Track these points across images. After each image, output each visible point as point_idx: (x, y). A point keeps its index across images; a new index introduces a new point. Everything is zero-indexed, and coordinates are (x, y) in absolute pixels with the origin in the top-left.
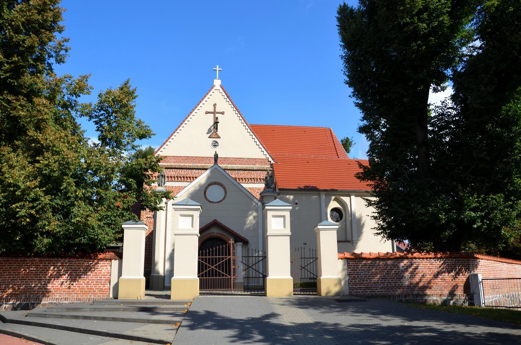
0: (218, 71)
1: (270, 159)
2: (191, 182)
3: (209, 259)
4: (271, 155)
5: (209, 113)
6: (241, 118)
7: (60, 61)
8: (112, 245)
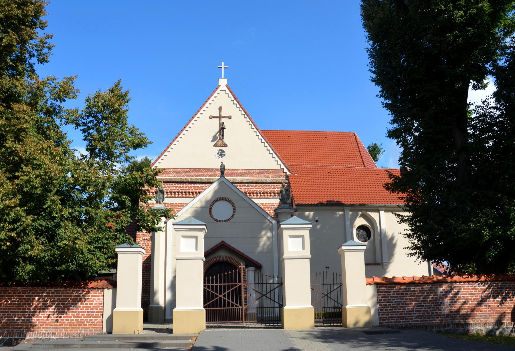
1: (286, 170)
3: (217, 286)
6: (251, 123)
7: (43, 60)
8: (103, 272)
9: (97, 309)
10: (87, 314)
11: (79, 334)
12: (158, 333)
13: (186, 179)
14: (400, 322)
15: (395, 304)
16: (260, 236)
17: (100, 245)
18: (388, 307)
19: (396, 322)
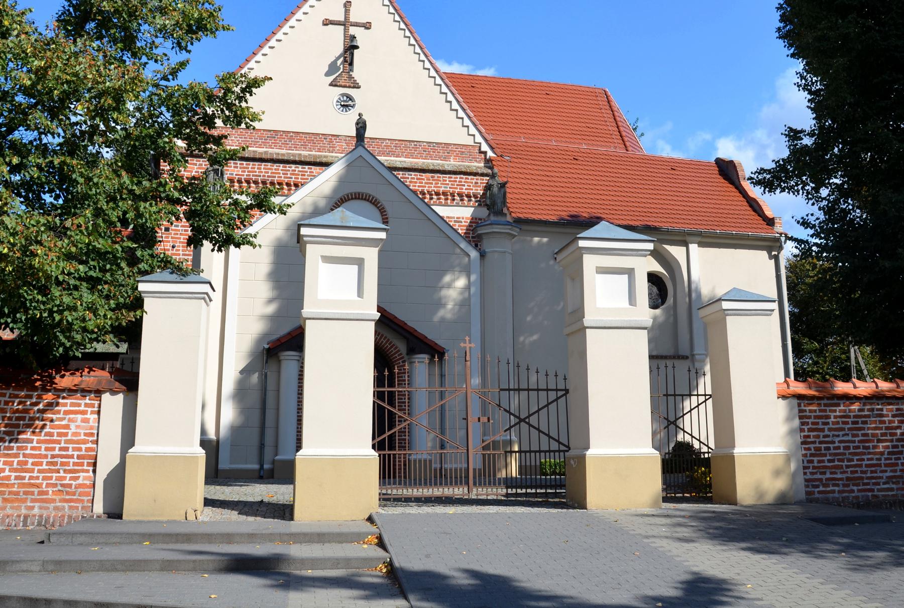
1: (485, 147)
4: (489, 137)
5: (332, 23)
6: (413, 41)
8: (100, 348)
9: (80, 449)
10: (48, 463)
11: (26, 517)
12: (251, 519)
13: (266, 153)
14: (853, 491)
15: (839, 448)
16: (440, 285)
17: (92, 273)
18: (825, 455)
19: (843, 492)
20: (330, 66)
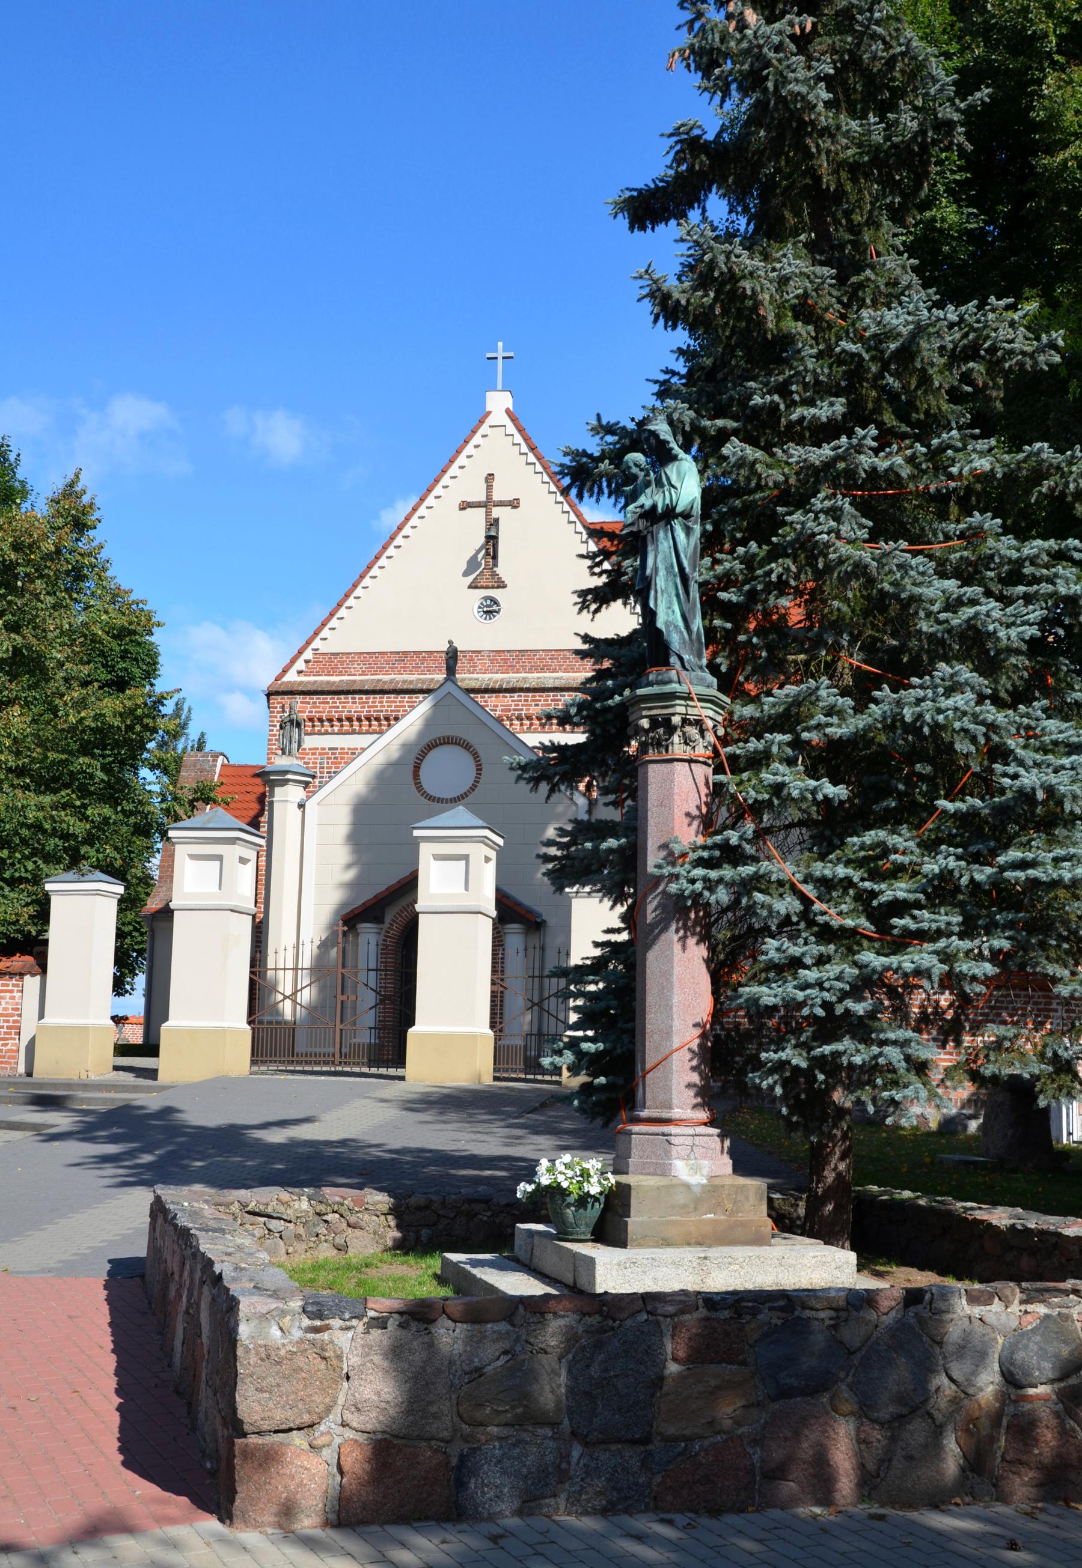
0: (500, 361)
2: (381, 733)
13: (392, 680)
20: (469, 562)
